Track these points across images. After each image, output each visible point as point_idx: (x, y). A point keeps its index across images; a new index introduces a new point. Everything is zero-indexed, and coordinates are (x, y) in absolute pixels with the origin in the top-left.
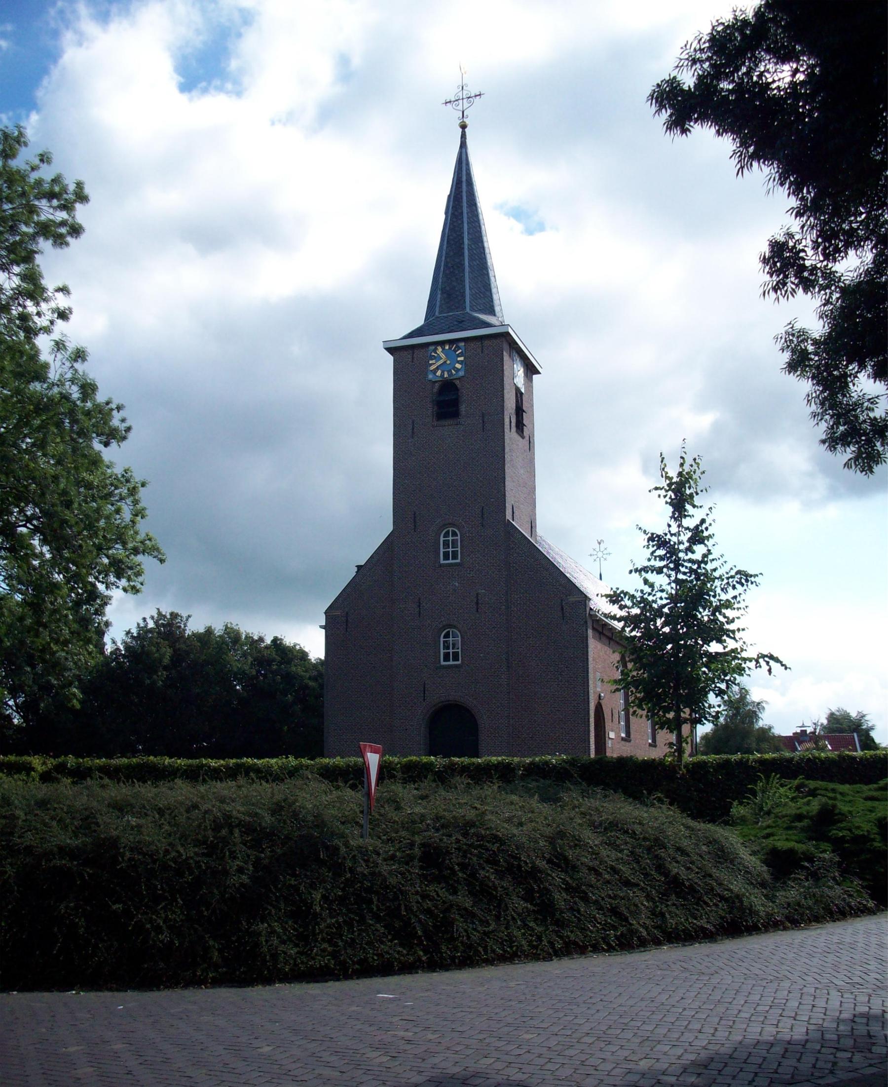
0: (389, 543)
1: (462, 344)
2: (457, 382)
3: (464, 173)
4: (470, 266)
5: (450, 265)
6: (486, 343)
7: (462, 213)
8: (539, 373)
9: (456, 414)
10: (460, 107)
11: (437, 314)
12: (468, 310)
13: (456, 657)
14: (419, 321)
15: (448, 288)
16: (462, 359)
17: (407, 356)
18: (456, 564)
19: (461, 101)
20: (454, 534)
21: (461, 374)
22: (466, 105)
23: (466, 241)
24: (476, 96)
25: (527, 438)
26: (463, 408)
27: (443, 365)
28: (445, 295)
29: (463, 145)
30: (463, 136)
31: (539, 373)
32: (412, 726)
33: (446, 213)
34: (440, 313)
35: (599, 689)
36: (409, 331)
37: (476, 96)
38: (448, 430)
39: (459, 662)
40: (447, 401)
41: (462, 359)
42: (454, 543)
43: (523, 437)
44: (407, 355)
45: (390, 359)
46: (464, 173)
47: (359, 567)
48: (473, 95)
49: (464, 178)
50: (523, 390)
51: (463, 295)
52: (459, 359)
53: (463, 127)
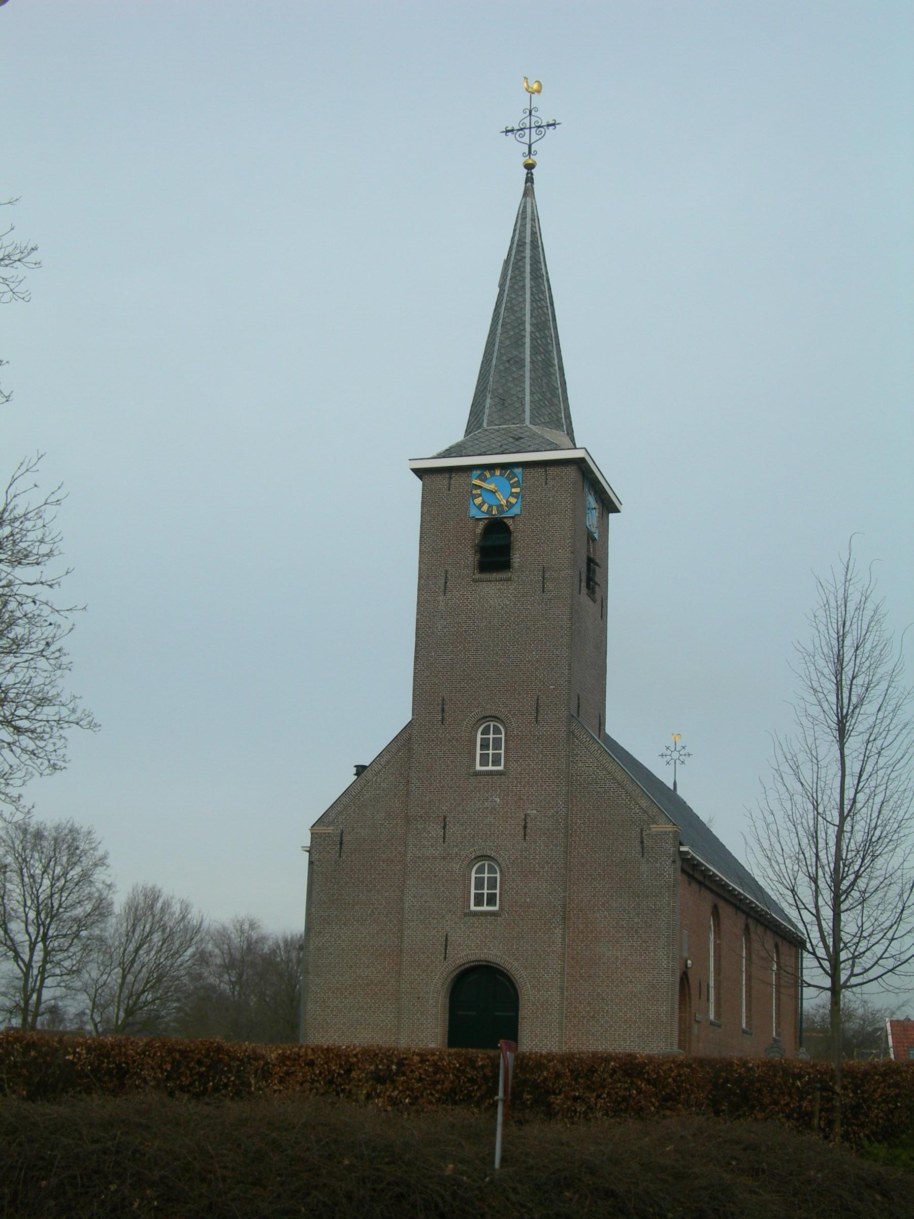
0: (404, 743)
1: (518, 471)
2: (510, 522)
3: (528, 226)
4: (532, 362)
5: (504, 358)
6: (552, 471)
7: (524, 286)
8: (618, 511)
9: (505, 565)
10: (526, 139)
11: (485, 425)
12: (527, 422)
13: (491, 900)
14: (457, 435)
15: (500, 391)
16: (517, 490)
17: (439, 481)
18: (499, 773)
19: (527, 131)
20: (497, 731)
21: (516, 510)
22: (535, 137)
23: (528, 327)
24: (549, 125)
25: (599, 602)
26: (516, 559)
27: (498, 496)
28: (496, 400)
29: (528, 192)
30: (530, 180)
31: (618, 511)
32: (427, 993)
33: (502, 285)
34: (490, 423)
35: (685, 955)
36: (447, 447)
37: (549, 125)
38: (494, 592)
39: (496, 908)
40: (495, 548)
41: (517, 490)
42: (497, 742)
43: (594, 601)
44: (441, 481)
45: (417, 484)
46: (528, 226)
47: (360, 770)
48: (544, 124)
49: (528, 240)
50: (596, 536)
51: (522, 400)
52: (514, 490)
53: (530, 167)
